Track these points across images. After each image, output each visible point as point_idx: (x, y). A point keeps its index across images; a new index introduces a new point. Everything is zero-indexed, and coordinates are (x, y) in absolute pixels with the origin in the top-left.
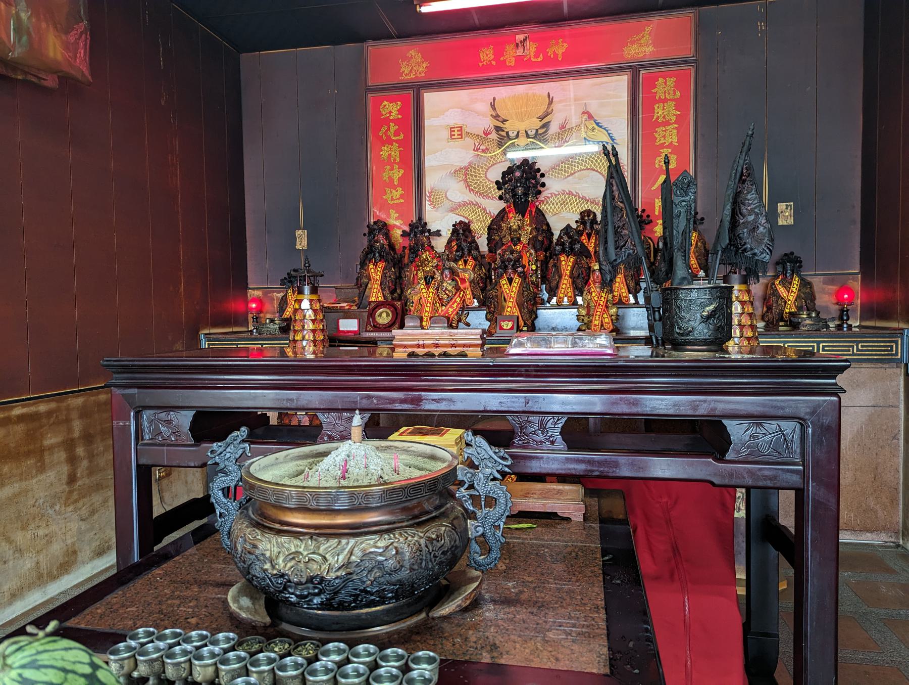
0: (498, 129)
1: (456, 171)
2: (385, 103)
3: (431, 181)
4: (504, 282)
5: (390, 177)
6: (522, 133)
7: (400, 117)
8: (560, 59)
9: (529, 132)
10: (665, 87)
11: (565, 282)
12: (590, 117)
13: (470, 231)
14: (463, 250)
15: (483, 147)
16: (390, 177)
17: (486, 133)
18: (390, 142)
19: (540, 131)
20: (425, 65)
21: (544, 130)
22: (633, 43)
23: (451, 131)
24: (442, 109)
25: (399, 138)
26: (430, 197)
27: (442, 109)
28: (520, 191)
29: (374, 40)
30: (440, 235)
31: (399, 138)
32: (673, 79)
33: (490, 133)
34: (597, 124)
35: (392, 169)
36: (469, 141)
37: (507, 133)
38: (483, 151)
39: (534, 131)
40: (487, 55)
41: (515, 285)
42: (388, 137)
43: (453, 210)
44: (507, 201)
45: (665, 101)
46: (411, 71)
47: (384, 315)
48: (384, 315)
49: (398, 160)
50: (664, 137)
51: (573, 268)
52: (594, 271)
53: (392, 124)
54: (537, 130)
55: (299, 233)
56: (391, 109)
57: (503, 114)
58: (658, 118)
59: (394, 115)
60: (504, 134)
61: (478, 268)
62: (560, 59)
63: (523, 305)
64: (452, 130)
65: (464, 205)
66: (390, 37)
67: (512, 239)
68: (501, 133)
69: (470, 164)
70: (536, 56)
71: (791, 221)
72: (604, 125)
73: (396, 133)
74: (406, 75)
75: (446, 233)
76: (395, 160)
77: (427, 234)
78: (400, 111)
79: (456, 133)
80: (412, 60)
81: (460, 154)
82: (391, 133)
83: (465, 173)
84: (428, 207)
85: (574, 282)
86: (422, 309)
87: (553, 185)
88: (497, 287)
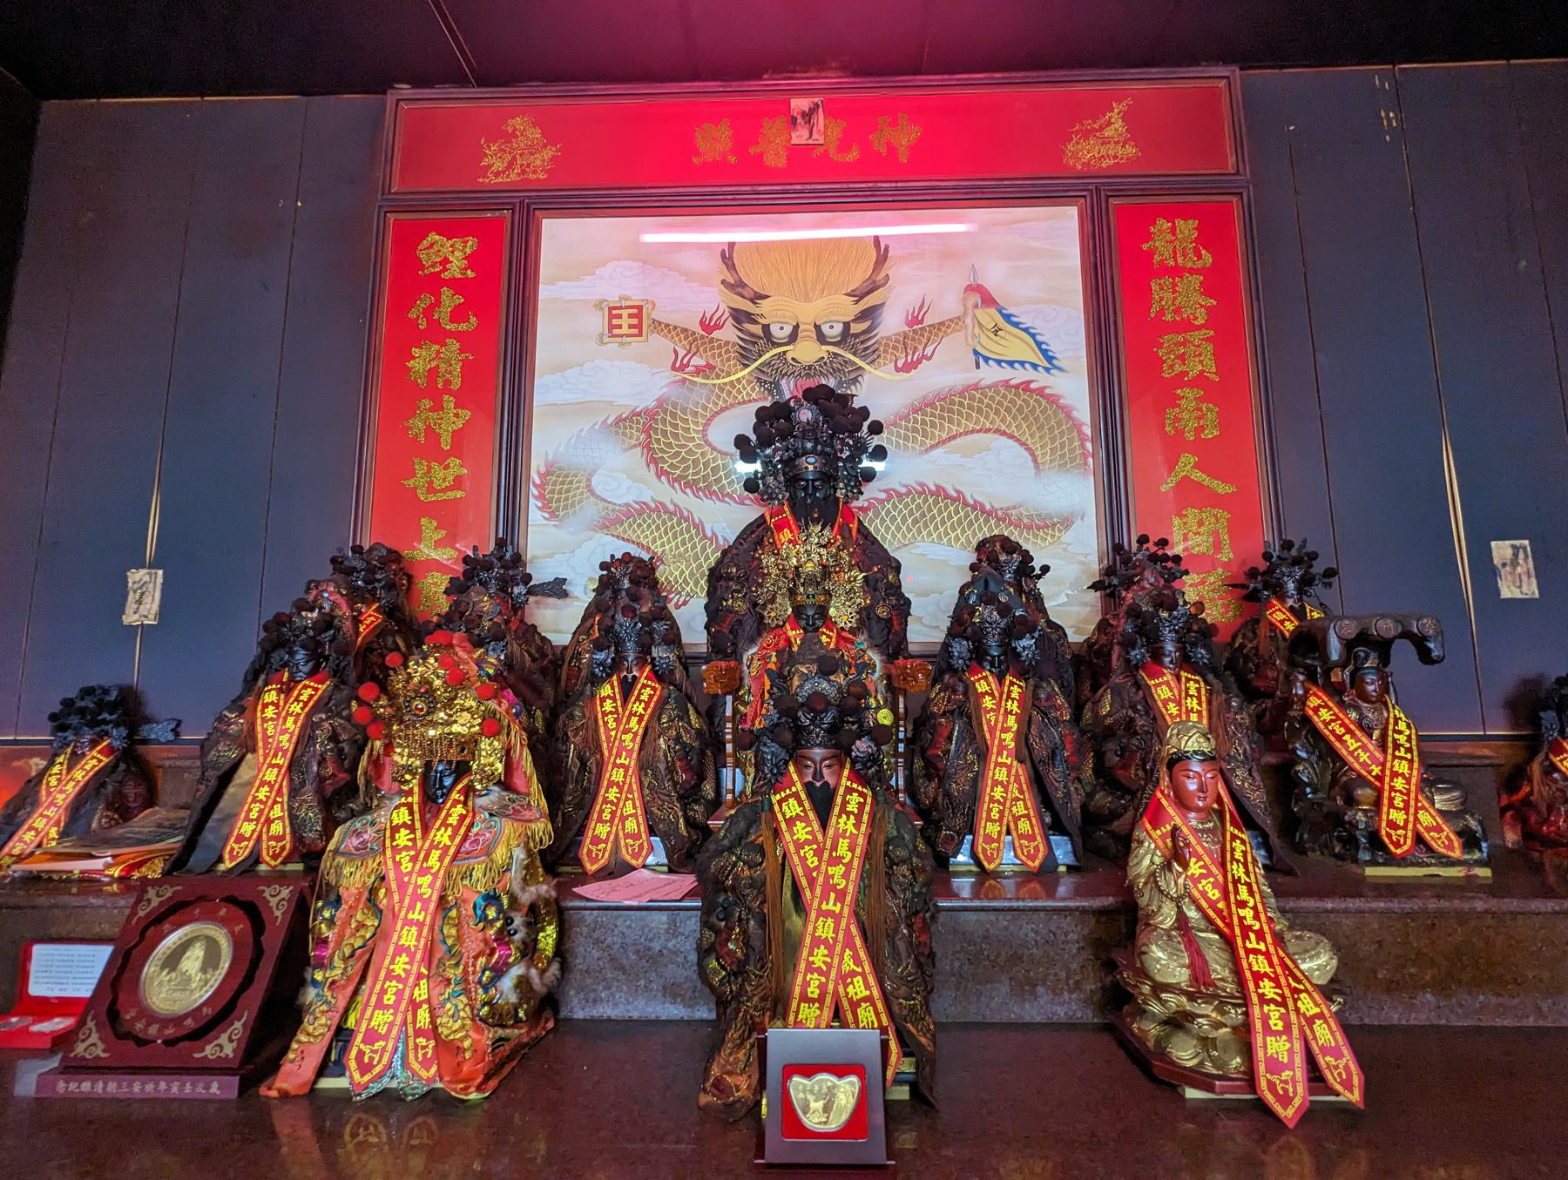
0: (740, 317)
1: (619, 420)
2: (434, 237)
3: (546, 443)
4: (791, 806)
5: (429, 429)
6: (807, 330)
7: (470, 273)
8: (903, 159)
9: (825, 329)
10: (1172, 239)
11: (1001, 775)
12: (988, 300)
13: (654, 584)
14: (619, 644)
15: (698, 361)
16: (429, 430)
17: (708, 326)
18: (436, 334)
19: (856, 328)
20: (548, 153)
21: (865, 325)
22: (1086, 135)
23: (611, 317)
24: (588, 264)
25: (463, 327)
26: (541, 487)
27: (588, 264)
28: (810, 465)
29: (418, 83)
30: (564, 594)
31: (463, 327)
32: (1193, 223)
33: (718, 327)
34: (1007, 318)
35: (438, 407)
36: (661, 346)
37: (766, 328)
38: (698, 371)
39: (839, 328)
40: (714, 142)
41: (847, 824)
42: (434, 325)
43: (609, 523)
44: (767, 497)
45: (1177, 271)
46: (511, 165)
47: (192, 961)
48: (192, 961)
49: (456, 384)
50: (1182, 358)
51: (1026, 722)
52: (1177, 761)
53: (446, 292)
54: (847, 325)
55: (136, 576)
56: (451, 255)
57: (754, 282)
58: (1162, 311)
59: (457, 267)
60: (757, 330)
61: (671, 710)
62: (903, 159)
63: (891, 936)
64: (613, 313)
65: (640, 513)
66: (460, 80)
67: (798, 611)
68: (748, 326)
69: (661, 402)
70: (844, 146)
71: (1531, 589)
72: (1026, 321)
73: (458, 315)
74: (497, 174)
75: (583, 594)
76: (447, 382)
77: (519, 590)
78: (472, 260)
79: (625, 321)
80: (516, 143)
81: (639, 377)
82: (443, 314)
83: (648, 429)
84: (535, 515)
85: (1039, 784)
86: (382, 935)
87: (897, 469)
88: (761, 836)
